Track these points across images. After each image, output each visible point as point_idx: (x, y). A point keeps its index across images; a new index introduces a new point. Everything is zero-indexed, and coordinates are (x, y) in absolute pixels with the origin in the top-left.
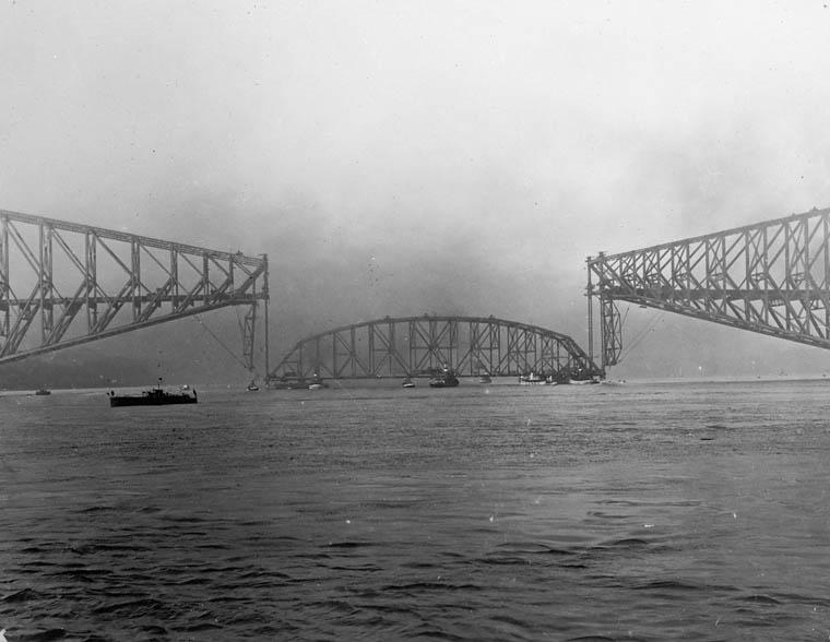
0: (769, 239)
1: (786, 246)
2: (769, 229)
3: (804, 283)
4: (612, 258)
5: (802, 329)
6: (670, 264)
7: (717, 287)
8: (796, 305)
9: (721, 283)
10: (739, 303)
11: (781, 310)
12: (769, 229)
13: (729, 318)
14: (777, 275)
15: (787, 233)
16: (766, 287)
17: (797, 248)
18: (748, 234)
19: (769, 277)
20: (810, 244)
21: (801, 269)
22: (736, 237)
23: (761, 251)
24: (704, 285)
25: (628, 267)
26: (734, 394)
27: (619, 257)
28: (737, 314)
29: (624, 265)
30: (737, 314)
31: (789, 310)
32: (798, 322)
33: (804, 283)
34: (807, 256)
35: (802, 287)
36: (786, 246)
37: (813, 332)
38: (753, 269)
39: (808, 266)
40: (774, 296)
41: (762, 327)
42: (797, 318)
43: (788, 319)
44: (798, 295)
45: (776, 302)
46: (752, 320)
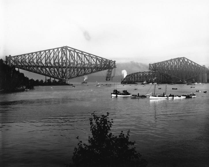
0: (51, 52)
1: (45, 56)
2: (42, 52)
3: (49, 64)
4: (12, 57)
5: (57, 76)
6: (45, 58)
7: (39, 65)
8: (47, 69)
9: (32, 64)
10: (60, 69)
11: (44, 70)
12: (42, 52)
13: (34, 71)
14: (44, 62)
15: (45, 53)
16: (41, 64)
17: (48, 56)
18: (37, 54)
19: (42, 62)
20: (42, 57)
21: (49, 61)
22: (43, 52)
23: (40, 57)
24: (45, 65)
25: (23, 59)
26: (142, 133)
27: (14, 57)
28: (43, 72)
29: (22, 58)
30: (43, 72)
31: (46, 70)
32: (57, 74)
33: (49, 64)
34: (50, 58)
35: (49, 65)
36: (45, 56)
37: (51, 74)
38: (38, 61)
39: (50, 61)
40: (42, 67)
41: (40, 73)
42: (56, 73)
43: (54, 73)
44: (48, 67)
45: (43, 68)
46: (46, 73)
